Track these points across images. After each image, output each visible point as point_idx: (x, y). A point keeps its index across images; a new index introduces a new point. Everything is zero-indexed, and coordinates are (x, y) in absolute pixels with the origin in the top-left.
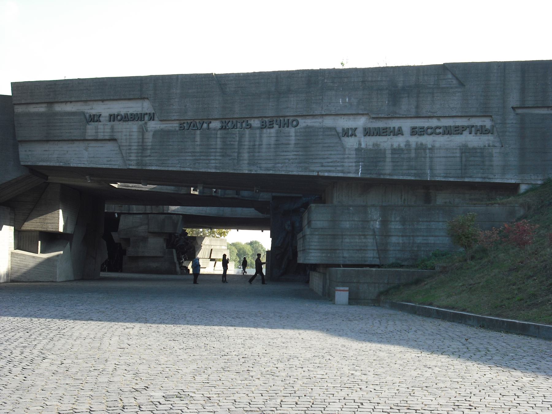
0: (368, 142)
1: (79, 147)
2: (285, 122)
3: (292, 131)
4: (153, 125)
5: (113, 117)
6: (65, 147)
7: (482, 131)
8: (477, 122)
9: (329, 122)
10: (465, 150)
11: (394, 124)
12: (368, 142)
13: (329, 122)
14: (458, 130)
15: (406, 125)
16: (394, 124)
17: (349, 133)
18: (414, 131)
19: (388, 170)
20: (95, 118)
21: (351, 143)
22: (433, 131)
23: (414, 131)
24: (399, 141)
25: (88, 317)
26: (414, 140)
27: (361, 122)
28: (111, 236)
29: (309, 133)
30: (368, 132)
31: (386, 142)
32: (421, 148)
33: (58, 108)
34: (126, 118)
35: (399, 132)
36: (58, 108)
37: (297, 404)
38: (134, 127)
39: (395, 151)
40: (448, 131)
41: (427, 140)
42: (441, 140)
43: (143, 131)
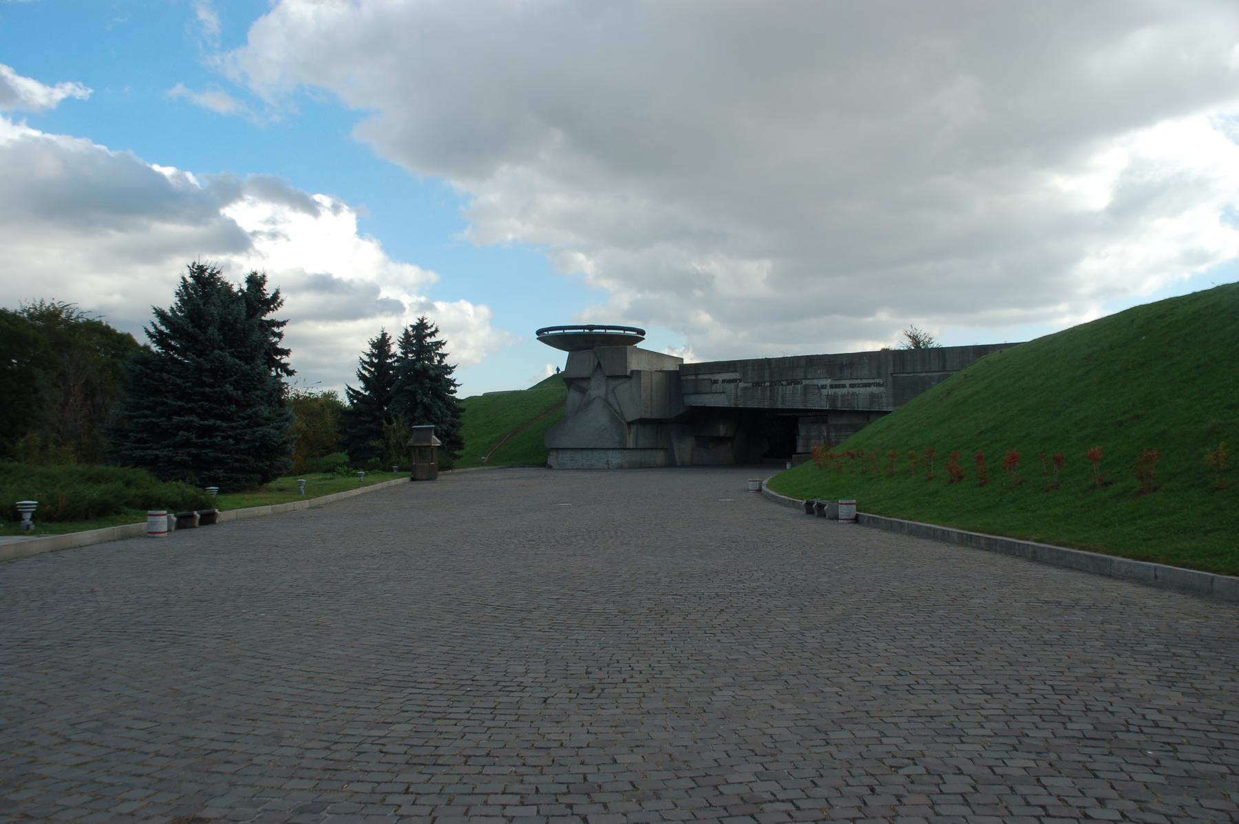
0: (831, 391)
1: (709, 396)
2: (797, 382)
3: (799, 387)
4: (741, 385)
5: (724, 381)
6: (703, 396)
7: (878, 385)
8: (877, 381)
9: (815, 382)
10: (872, 395)
11: (842, 382)
12: (831, 391)
13: (815, 382)
14: (869, 385)
15: (847, 383)
16: (842, 382)
17: (824, 387)
18: (852, 386)
19: (839, 405)
20: (716, 382)
21: (824, 392)
22: (859, 386)
23: (852, 386)
24: (845, 391)
25: (991, 357)
26: (851, 390)
27: (828, 382)
28: (471, 400)
29: (806, 387)
30: (832, 387)
31: (840, 391)
32: (854, 394)
33: (700, 377)
34: (730, 381)
35: (843, 386)
36: (700, 377)
37: (872, 790)
38: (732, 385)
39: (843, 396)
40: (866, 385)
41: (856, 390)
42: (862, 390)
43: (737, 387)
